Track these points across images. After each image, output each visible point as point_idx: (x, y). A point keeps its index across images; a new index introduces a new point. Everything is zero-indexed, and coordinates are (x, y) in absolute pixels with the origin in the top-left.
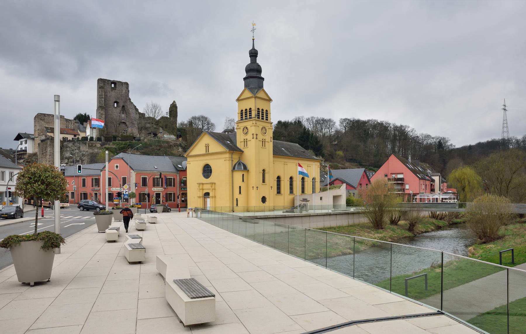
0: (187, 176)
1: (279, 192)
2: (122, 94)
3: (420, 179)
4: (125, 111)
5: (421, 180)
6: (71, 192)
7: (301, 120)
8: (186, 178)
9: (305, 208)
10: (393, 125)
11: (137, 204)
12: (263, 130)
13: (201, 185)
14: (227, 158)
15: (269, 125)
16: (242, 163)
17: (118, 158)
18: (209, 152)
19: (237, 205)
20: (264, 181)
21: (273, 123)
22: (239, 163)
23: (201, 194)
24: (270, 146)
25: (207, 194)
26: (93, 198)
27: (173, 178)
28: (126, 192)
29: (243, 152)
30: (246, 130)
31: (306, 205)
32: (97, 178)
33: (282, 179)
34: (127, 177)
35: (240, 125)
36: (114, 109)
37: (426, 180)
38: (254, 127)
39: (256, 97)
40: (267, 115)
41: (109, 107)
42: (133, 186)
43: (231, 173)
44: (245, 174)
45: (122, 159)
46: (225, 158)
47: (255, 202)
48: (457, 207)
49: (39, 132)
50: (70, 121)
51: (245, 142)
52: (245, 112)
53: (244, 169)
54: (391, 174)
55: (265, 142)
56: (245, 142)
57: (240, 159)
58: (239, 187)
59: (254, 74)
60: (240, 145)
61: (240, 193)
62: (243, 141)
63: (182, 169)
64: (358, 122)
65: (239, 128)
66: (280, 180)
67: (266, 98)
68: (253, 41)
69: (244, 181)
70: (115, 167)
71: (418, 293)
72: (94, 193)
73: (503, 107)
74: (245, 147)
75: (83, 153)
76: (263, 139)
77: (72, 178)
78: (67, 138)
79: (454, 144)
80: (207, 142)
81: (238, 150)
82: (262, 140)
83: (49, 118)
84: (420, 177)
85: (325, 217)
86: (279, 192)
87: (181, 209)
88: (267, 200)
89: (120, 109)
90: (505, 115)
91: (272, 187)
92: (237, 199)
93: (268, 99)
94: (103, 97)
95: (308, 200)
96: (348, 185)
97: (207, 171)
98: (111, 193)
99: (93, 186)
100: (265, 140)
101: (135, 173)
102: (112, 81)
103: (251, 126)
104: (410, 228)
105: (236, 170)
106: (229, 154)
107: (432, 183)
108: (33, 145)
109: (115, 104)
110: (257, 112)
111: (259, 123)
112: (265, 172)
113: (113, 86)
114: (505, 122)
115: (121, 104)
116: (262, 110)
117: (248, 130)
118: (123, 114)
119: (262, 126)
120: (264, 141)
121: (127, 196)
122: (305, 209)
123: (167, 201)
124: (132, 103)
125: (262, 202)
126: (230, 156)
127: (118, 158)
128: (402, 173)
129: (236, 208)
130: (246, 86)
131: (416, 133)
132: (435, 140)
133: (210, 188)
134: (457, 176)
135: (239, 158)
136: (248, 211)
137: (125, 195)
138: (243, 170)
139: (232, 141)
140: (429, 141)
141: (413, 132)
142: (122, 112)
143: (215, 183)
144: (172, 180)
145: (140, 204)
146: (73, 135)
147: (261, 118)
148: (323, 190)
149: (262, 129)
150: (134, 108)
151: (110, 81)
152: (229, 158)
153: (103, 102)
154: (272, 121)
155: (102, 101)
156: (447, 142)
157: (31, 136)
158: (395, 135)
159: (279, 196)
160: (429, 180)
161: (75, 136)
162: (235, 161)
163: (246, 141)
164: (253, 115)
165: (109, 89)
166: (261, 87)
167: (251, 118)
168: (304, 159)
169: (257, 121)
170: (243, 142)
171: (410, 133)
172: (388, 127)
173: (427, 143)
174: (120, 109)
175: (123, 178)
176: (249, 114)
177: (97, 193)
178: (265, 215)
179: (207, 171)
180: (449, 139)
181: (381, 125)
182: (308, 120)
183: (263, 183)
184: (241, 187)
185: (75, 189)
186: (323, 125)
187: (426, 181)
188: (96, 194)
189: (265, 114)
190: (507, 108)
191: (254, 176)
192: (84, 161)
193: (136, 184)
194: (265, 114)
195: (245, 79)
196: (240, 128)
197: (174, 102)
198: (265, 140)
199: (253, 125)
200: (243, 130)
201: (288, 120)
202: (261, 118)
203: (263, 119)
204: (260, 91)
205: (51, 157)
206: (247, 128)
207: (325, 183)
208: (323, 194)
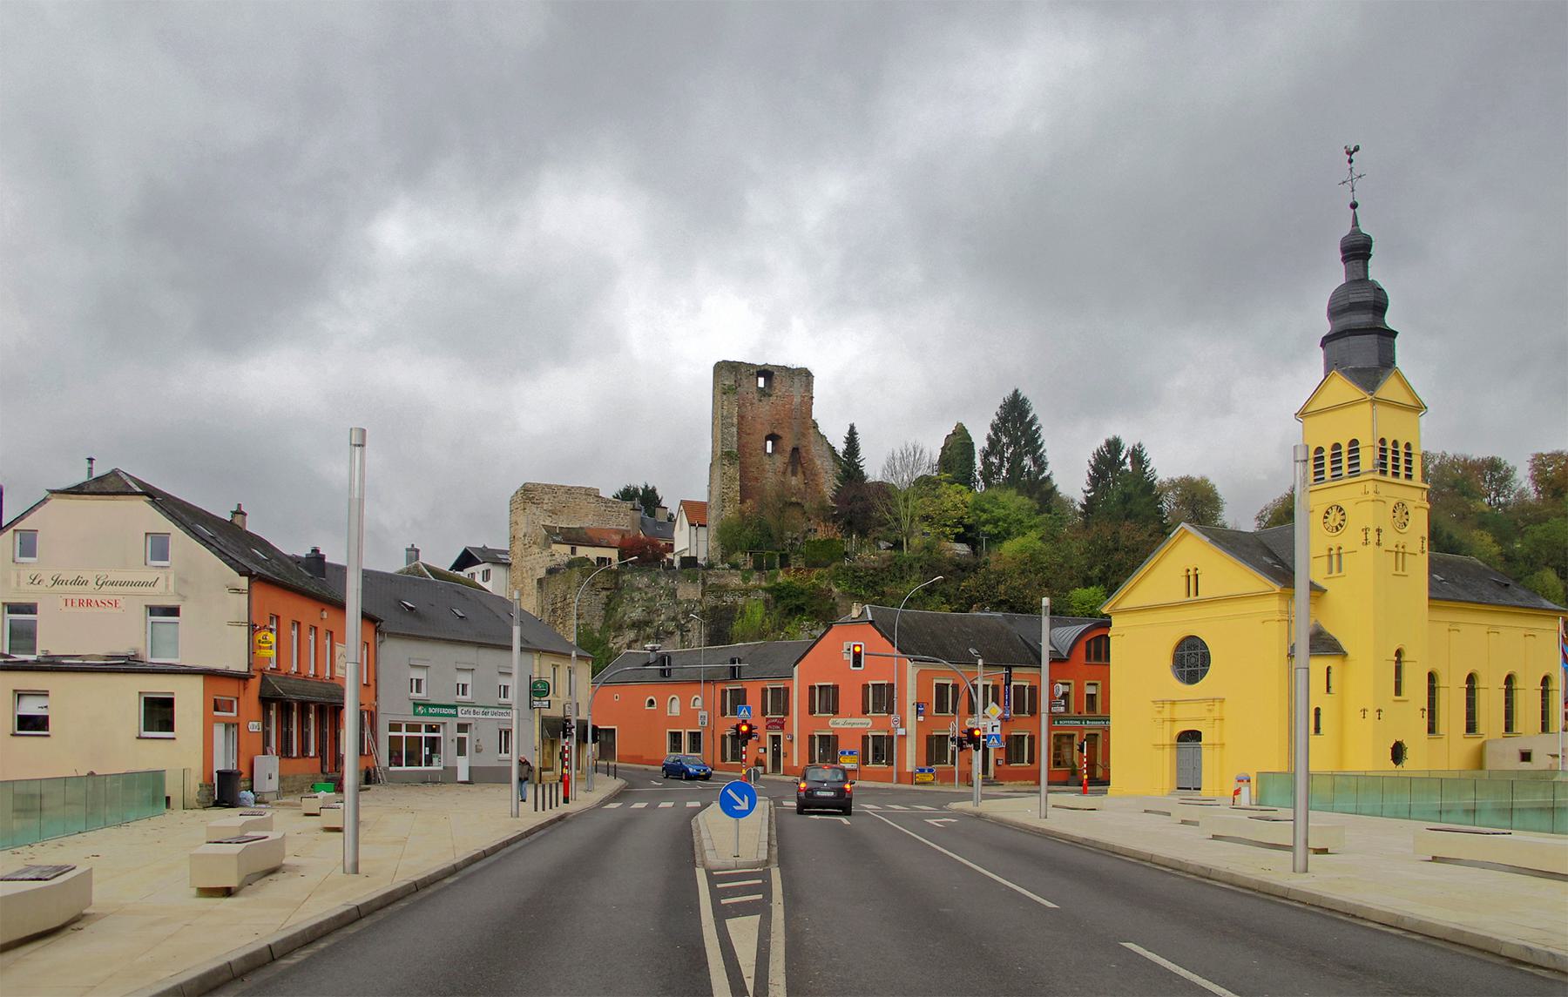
2: (792, 410)
4: (799, 465)
6: (687, 731)
11: (922, 771)
12: (1398, 514)
20: (1398, 691)
23: (1168, 735)
24: (1419, 565)
27: (1027, 684)
28: (993, 727)
30: (1334, 518)
32: (782, 686)
36: (766, 460)
41: (751, 454)
44: (1333, 662)
51: (1330, 556)
52: (1333, 455)
55: (1403, 553)
56: (1335, 558)
59: (1363, 319)
62: (1326, 553)
66: (1436, 685)
67: (1405, 399)
69: (1332, 690)
72: (768, 734)
74: (1331, 572)
76: (1396, 546)
83: (554, 497)
87: (1089, 788)
88: (1409, 753)
89: (780, 461)
93: (1412, 403)
94: (735, 420)
98: (829, 736)
99: (868, 712)
100: (1403, 547)
101: (917, 670)
109: (769, 443)
115: (788, 444)
116: (1395, 443)
117: (1344, 514)
118: (792, 475)
119: (1396, 500)
120: (1402, 550)
121: (996, 741)
123: (1008, 762)
124: (823, 437)
137: (991, 735)
142: (789, 469)
143: (1222, 700)
145: (930, 771)
147: (1402, 475)
149: (1394, 511)
150: (828, 454)
152: (1280, 611)
153: (735, 439)
155: (732, 437)
157: (500, 556)
163: (1335, 558)
166: (1387, 362)
169: (1379, 484)
170: (1326, 558)
177: (781, 734)
184: (1321, 712)
188: (776, 739)
192: (690, 634)
193: (918, 706)
195: (1325, 342)
198: (1403, 547)
200: (1326, 517)
202: (1402, 475)
203: (1396, 475)
206: (1341, 509)
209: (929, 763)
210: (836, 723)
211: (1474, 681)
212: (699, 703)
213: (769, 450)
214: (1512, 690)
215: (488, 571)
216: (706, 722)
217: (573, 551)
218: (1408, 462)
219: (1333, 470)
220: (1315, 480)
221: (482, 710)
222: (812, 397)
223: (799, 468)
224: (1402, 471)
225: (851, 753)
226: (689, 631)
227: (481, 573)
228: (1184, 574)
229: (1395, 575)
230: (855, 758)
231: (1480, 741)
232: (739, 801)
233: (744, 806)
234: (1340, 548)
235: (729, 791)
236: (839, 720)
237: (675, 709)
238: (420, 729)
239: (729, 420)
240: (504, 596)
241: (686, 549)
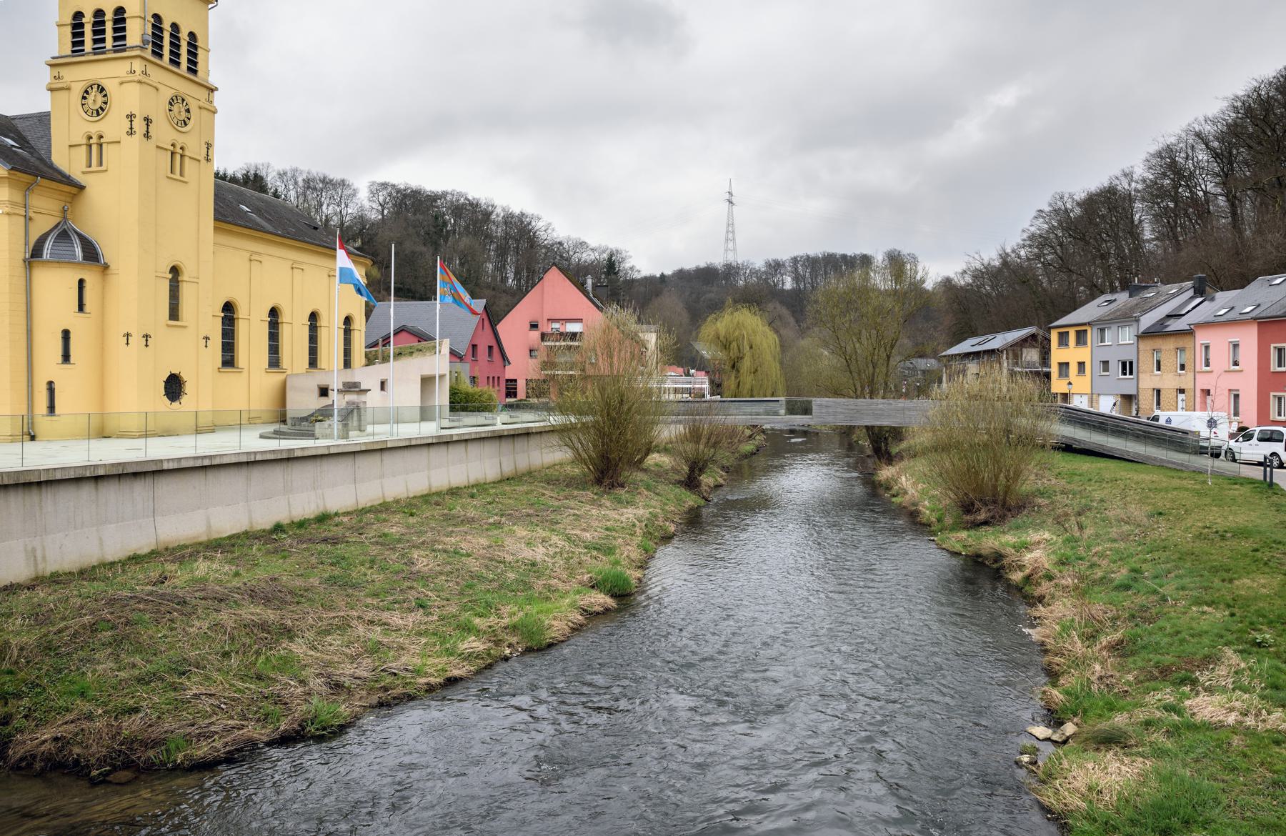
1: (229, 361)
7: (263, 173)
9: (355, 418)
10: (504, 210)
12: (175, 108)
15: (203, 94)
16: (76, 232)
19: (52, 408)
20: (174, 314)
21: (216, 89)
22: (64, 235)
29: (82, 188)
30: (95, 99)
31: (362, 406)
35: (69, 74)
38: (138, 86)
40: (195, 55)
43: (20, 269)
44: (91, 278)
48: (783, 412)
53: (85, 258)
54: (548, 320)
55: (182, 156)
56: (95, 148)
57: (65, 218)
58: (60, 336)
60: (65, 157)
61: (66, 357)
62: (84, 141)
64: (416, 194)
65: (64, 85)
66: (235, 316)
69: (87, 308)
73: (727, 196)
74: (90, 166)
79: (638, 268)
82: (172, 148)
85: (434, 452)
86: (229, 361)
88: (188, 388)
90: (730, 215)
91: (207, 338)
92: (50, 383)
95: (363, 387)
103: (121, 83)
104: (689, 477)
105: (48, 261)
106: (11, 186)
110: (149, 31)
112: (180, 279)
114: (730, 229)
117: (105, 96)
120: (181, 151)
122: (355, 423)
125: (169, 399)
128: (580, 320)
129: (44, 423)
131: (555, 234)
132: (597, 254)
134: (722, 332)
135: (64, 211)
136: (104, 435)
138: (79, 263)
139: (28, 143)
140: (584, 255)
141: (549, 231)
152: (12, 203)
154: (213, 80)
156: (623, 260)
158: (507, 237)
159: (229, 376)
162: (43, 224)
163: (95, 146)
167: (123, 48)
168: (320, 249)
170: (84, 148)
171: (541, 233)
172: (492, 212)
173: (579, 260)
176: (115, 30)
178: (200, 452)
180: (628, 254)
181: (474, 206)
182: (282, 175)
183: (170, 319)
184: (72, 336)
186: (324, 194)
190: (734, 200)
196: (68, 89)
199: (132, 77)
201: (225, 169)
206: (103, 89)
211: (277, 315)
214: (278, 323)
220: (73, 52)
229: (168, 177)
231: (282, 377)
234: (102, 137)
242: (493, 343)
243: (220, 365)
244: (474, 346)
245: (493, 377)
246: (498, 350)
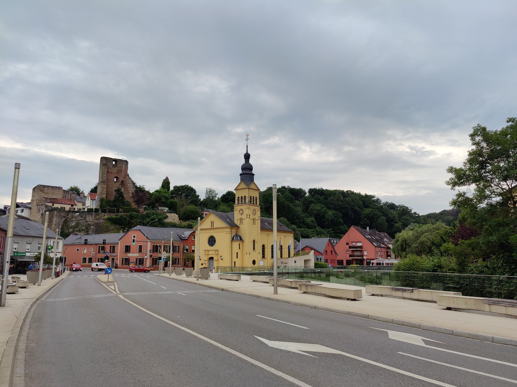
0: (195, 244)
1: (264, 257)
3: (376, 247)
5: (376, 248)
8: (194, 245)
11: (151, 267)
13: (207, 251)
14: (228, 231)
17: (136, 230)
18: (214, 227)
20: (254, 249)
23: (207, 258)
24: (258, 223)
25: (212, 258)
26: (110, 262)
29: (239, 227)
30: (241, 211)
33: (266, 247)
34: (143, 245)
37: (381, 247)
39: (249, 188)
42: (292, 252)
43: (231, 242)
45: (140, 230)
46: (227, 232)
47: (248, 264)
49: (37, 202)
50: (67, 192)
56: (241, 220)
61: (237, 257)
62: (240, 219)
63: (185, 238)
68: (247, 147)
69: (240, 249)
70: (133, 237)
71: (297, 252)
75: (89, 223)
77: (91, 245)
78: (65, 208)
80: (212, 220)
81: (235, 225)
84: (376, 245)
86: (264, 257)
88: (256, 262)
91: (259, 253)
93: (257, 189)
94: (106, 173)
96: (315, 250)
97: (212, 241)
98: (127, 258)
102: (114, 159)
106: (230, 229)
107: (387, 250)
108: (30, 213)
109: (115, 179)
111: (251, 207)
113: (114, 163)
115: (121, 179)
116: (253, 197)
119: (253, 209)
124: (130, 178)
126: (230, 230)
127: (136, 230)
130: (241, 180)
133: (214, 253)
135: (236, 231)
143: (218, 250)
144: (169, 247)
145: (153, 267)
146: (71, 205)
148: (297, 254)
150: (131, 183)
151: (112, 159)
160: (385, 248)
161: (72, 206)
162: (234, 234)
163: (241, 220)
164: (247, 201)
165: (111, 166)
166: (252, 180)
170: (239, 220)
174: (119, 183)
175: (139, 246)
179: (212, 241)
184: (238, 253)
185: (93, 255)
187: (382, 248)
189: (255, 200)
191: (248, 244)
194: (255, 200)
195: (241, 175)
197: (167, 178)
202: (255, 204)
203: (253, 204)
204: (251, 184)
205: (56, 226)
207: (297, 250)
208: (297, 258)
209: (152, 265)
210: (130, 255)
212: (92, 250)
213: (115, 180)
215: (23, 210)
216: (94, 255)
217: (53, 205)
218: (256, 201)
219: (241, 202)
221: (33, 253)
222: (128, 168)
223: (123, 186)
224: (255, 203)
225: (133, 262)
226: (89, 229)
227: (20, 210)
228: (211, 222)
230: (134, 264)
232: (109, 271)
233: (110, 272)
235: (107, 269)
236: (130, 254)
237: (85, 251)
238: (347, 262)
239: (104, 173)
240: (28, 217)
241: (89, 206)
242: (332, 250)
243: (262, 257)
244: (326, 251)
245: (333, 260)
246: (334, 252)
